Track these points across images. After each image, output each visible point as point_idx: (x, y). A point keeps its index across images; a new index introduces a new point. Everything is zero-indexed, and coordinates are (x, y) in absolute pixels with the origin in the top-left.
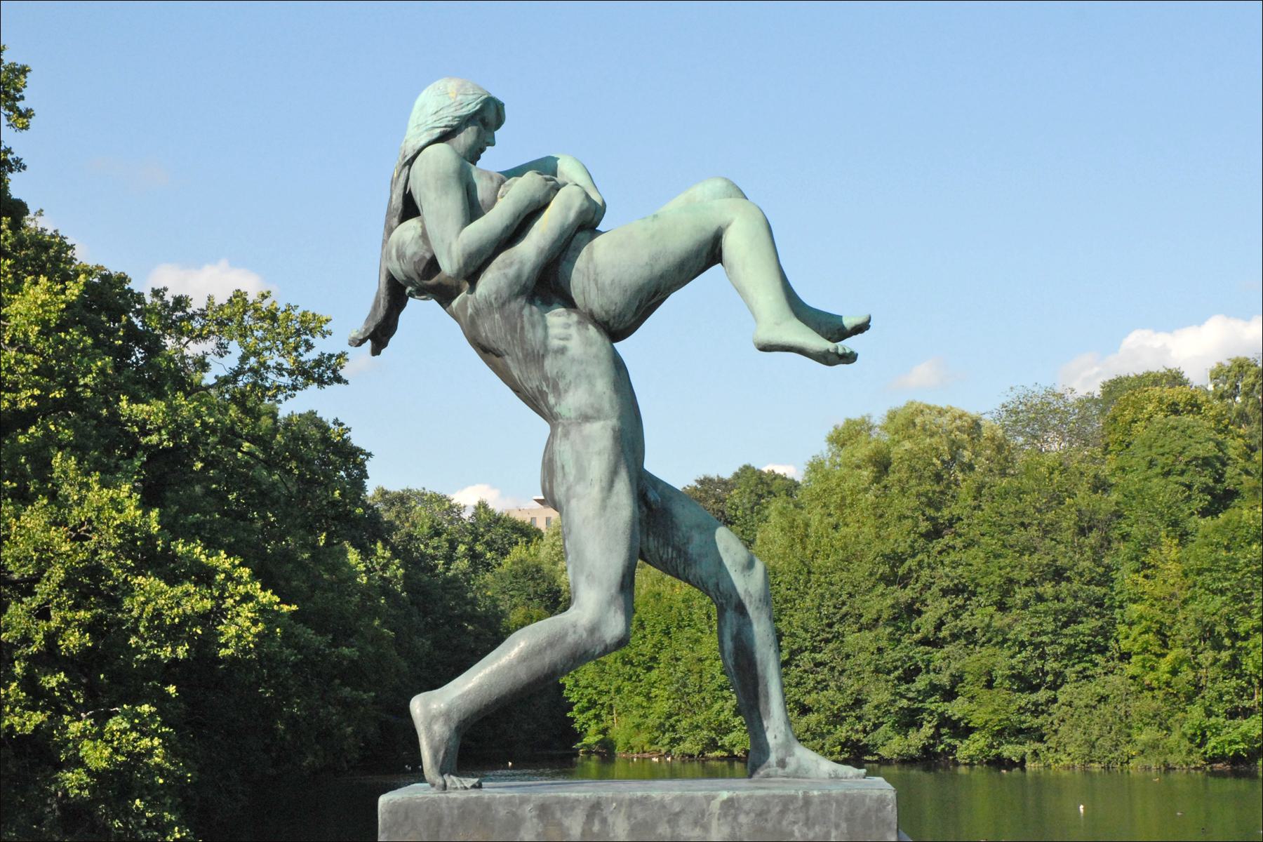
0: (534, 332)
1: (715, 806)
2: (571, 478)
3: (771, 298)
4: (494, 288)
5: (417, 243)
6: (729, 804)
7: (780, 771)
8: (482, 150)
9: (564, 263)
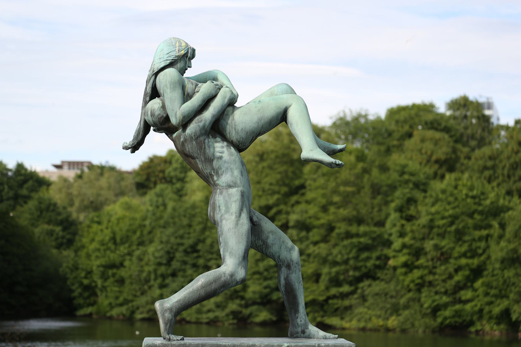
0: (209, 150)
2: (223, 211)
3: (308, 139)
4: (194, 131)
5: (160, 110)
7: (302, 335)
8: (186, 69)
9: (222, 120)
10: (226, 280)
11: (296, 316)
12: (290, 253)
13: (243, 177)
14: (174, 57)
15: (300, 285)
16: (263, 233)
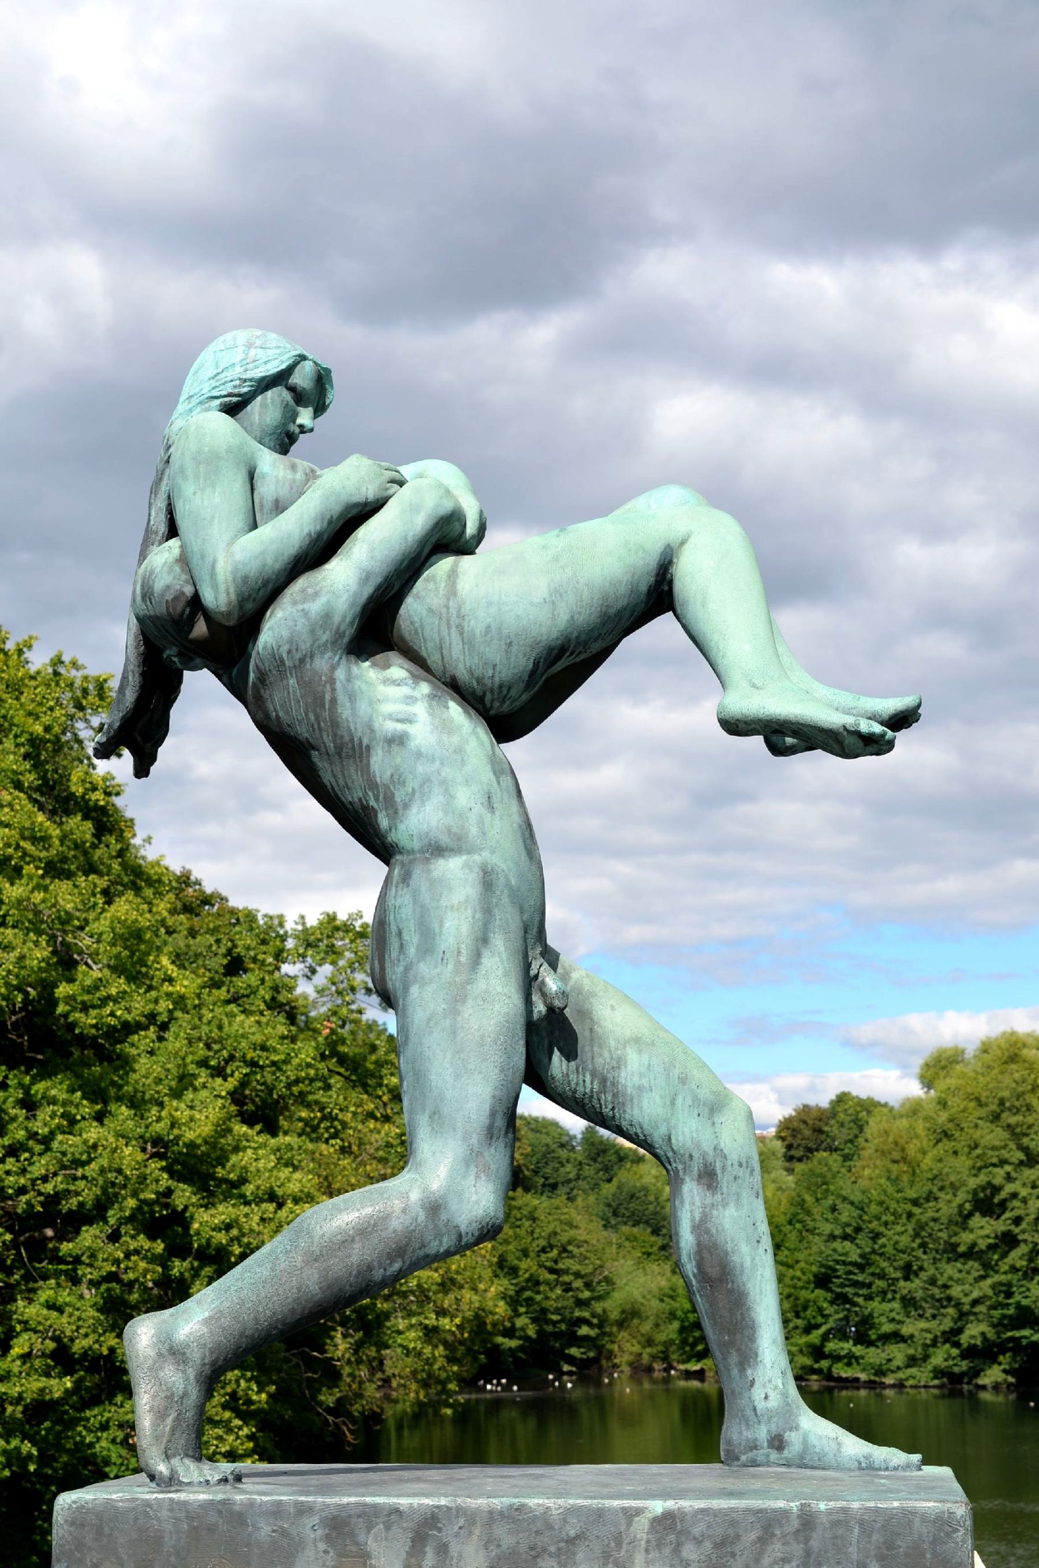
1: (641, 1527)
2: (412, 951)
6: (666, 1522)
7: (774, 1456)
10: (412, 1228)
11: (746, 1377)
12: (713, 1124)
13: (497, 814)
14: (235, 387)
15: (761, 1251)
16: (601, 1047)
